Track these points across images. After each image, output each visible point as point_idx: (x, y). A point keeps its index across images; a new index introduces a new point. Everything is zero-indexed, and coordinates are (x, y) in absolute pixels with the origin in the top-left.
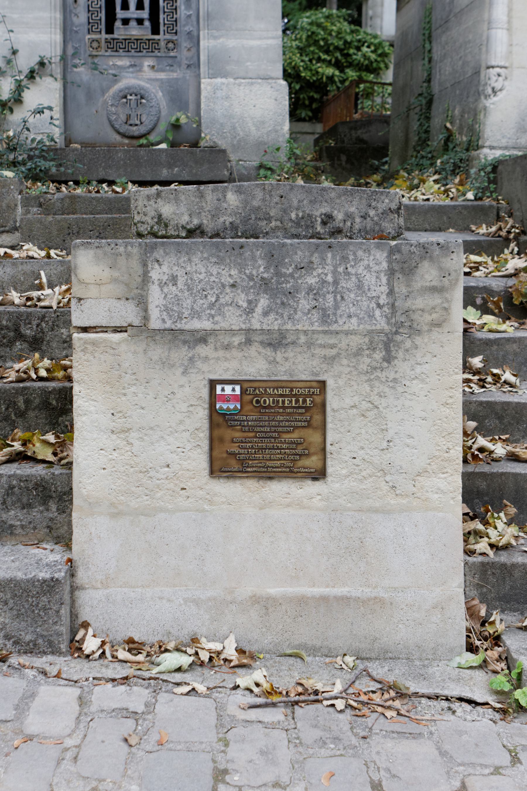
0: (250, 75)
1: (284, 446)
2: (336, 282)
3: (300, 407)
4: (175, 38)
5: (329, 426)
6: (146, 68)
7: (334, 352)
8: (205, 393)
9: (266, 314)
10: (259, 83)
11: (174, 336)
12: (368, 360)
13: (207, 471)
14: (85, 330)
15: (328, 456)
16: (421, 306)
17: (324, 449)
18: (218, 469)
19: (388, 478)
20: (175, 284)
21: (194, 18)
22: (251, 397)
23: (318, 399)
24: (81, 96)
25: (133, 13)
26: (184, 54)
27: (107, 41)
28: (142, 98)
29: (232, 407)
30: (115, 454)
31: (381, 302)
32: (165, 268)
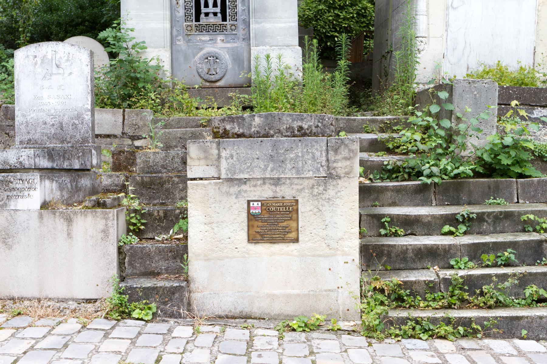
0: (280, 44)
1: (280, 228)
2: (303, 156)
3: (287, 211)
4: (236, 23)
5: (300, 219)
6: (219, 41)
7: (302, 187)
8: (246, 206)
9: (272, 171)
10: (284, 49)
12: (316, 190)
13: (247, 240)
14: (192, 179)
15: (300, 232)
16: (341, 166)
17: (298, 230)
18: (252, 239)
19: (326, 242)
20: (232, 159)
21: (247, 11)
22: (265, 207)
23: (295, 208)
24: (181, 59)
25: (211, 9)
26: (241, 32)
28: (217, 58)
29: (257, 212)
30: (206, 233)
31: (323, 164)
32: (228, 152)
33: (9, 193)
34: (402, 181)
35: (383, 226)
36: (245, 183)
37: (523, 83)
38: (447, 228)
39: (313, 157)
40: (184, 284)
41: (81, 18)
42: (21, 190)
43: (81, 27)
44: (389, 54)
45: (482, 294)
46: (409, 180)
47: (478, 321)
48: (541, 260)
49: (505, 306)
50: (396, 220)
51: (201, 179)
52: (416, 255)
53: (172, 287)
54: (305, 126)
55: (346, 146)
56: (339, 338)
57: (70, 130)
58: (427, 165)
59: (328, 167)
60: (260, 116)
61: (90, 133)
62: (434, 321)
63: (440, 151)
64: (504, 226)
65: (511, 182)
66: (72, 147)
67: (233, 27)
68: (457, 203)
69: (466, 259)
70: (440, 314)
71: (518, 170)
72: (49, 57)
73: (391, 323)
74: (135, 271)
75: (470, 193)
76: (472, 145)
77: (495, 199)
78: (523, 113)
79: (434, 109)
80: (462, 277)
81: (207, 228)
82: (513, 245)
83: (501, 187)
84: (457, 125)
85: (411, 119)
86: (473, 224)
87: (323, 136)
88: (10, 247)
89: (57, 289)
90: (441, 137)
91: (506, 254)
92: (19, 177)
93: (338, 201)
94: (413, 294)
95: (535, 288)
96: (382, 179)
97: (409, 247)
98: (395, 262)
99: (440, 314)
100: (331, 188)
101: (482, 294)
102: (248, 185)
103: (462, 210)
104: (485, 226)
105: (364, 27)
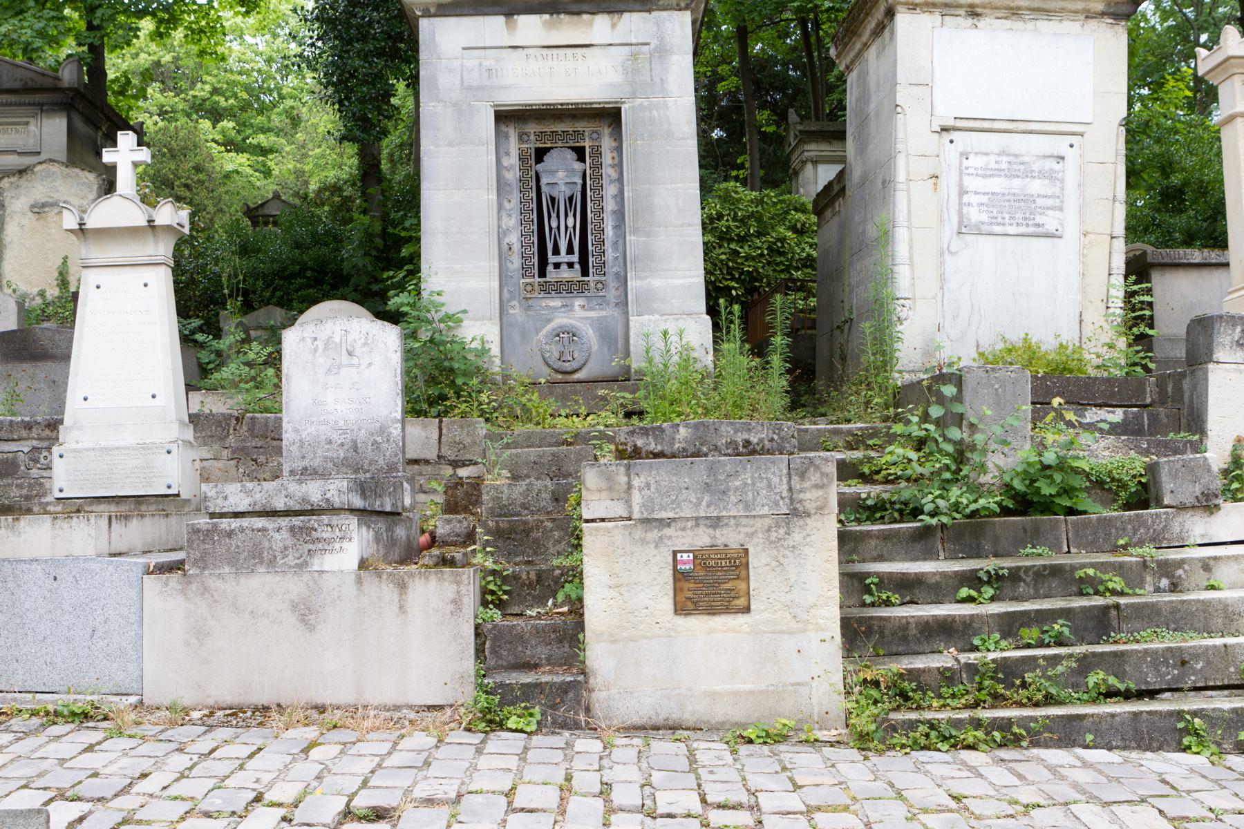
0: (676, 311)
2: (753, 484)
5: (752, 578)
6: (576, 307)
7: (753, 529)
8: (670, 559)
9: (708, 506)
11: (646, 521)
13: (672, 611)
14: (587, 521)
18: (681, 609)
21: (621, 260)
23: (744, 561)
24: (517, 337)
25: (564, 257)
26: (612, 293)
27: (540, 284)
32: (642, 479)
33: (311, 546)
34: (890, 523)
35: (867, 590)
36: (669, 525)
37: (1065, 369)
38: (964, 592)
39: (769, 485)
40: (581, 678)
41: (298, 263)
42: (329, 541)
43: (299, 281)
44: (847, 325)
45: (1024, 685)
46: (901, 521)
47: (1021, 723)
48: (1109, 636)
49: (1060, 703)
50: (886, 581)
51: (603, 520)
52: (921, 632)
53: (563, 682)
54: (755, 440)
55: (817, 467)
56: (819, 751)
57: (369, 453)
58: (930, 497)
59: (791, 499)
60: (687, 426)
61: (401, 456)
62: (957, 724)
63: (947, 475)
64: (1050, 586)
65: (1058, 521)
66: (373, 478)
67: (600, 286)
68: (978, 556)
69: (998, 636)
70: (965, 715)
71: (1065, 502)
72: (337, 340)
73: (894, 729)
74: (500, 662)
75: (996, 540)
76: (996, 465)
77: (1034, 547)
78: (1070, 416)
79: (936, 411)
80: (994, 661)
81: (614, 593)
82: (1066, 613)
83: (1042, 529)
84: (970, 436)
85: (898, 428)
86: (1003, 584)
87: (781, 453)
88: (311, 628)
89: (383, 691)
90: (948, 454)
91: (1056, 627)
92: (326, 522)
93: (807, 550)
94: (921, 688)
95: (1101, 675)
96: (859, 521)
97: (911, 620)
98: (891, 643)
99: (965, 715)
100: (797, 530)
101: (1024, 685)
102: (673, 528)
103: (987, 565)
104: (1022, 588)
105: (782, 271)
